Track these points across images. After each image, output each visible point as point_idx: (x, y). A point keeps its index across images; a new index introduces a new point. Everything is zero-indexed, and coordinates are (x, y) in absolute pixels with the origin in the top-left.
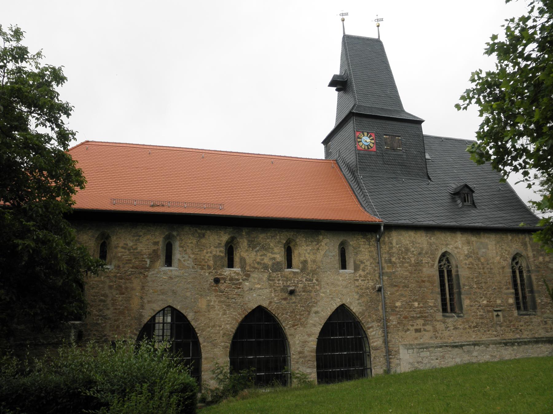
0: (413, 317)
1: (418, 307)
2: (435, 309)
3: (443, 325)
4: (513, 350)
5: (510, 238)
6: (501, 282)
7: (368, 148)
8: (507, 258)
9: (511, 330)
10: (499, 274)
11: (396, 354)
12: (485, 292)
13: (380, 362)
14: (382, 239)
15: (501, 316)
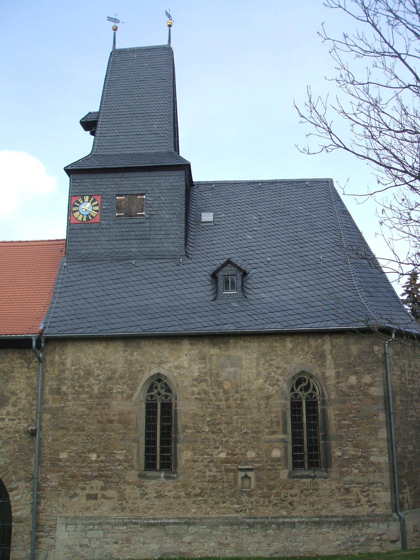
0: (86, 476)
1: (96, 461)
2: (126, 464)
3: (137, 490)
4: (265, 536)
5: (289, 345)
6: (260, 423)
7: (88, 219)
8: (278, 380)
9: (270, 502)
10: (259, 407)
11: (51, 531)
12: (224, 439)
13: (23, 541)
14: (48, 358)
15: (253, 480)
